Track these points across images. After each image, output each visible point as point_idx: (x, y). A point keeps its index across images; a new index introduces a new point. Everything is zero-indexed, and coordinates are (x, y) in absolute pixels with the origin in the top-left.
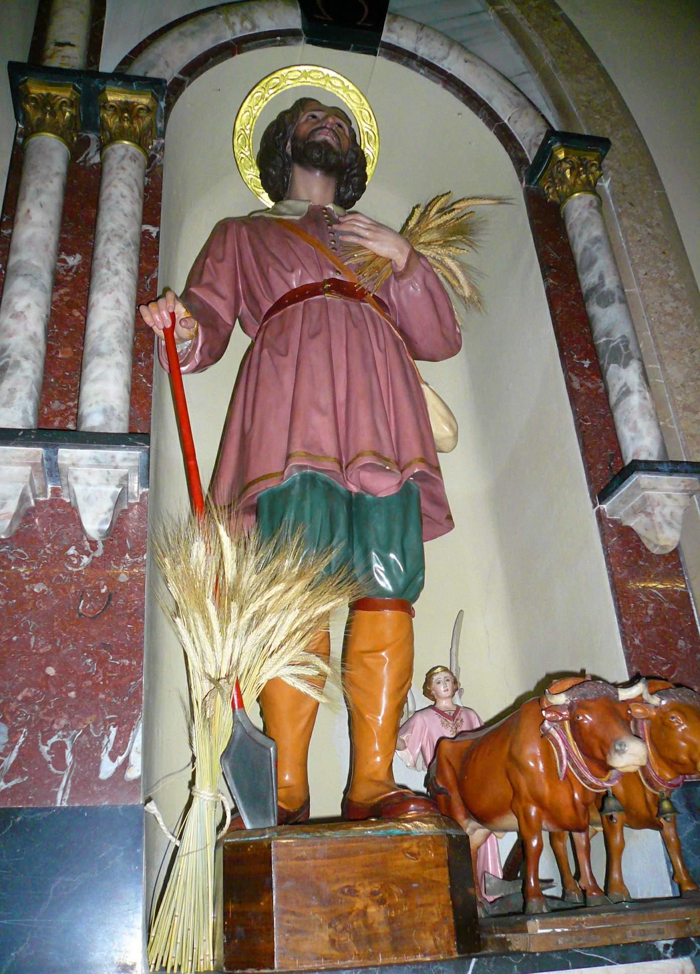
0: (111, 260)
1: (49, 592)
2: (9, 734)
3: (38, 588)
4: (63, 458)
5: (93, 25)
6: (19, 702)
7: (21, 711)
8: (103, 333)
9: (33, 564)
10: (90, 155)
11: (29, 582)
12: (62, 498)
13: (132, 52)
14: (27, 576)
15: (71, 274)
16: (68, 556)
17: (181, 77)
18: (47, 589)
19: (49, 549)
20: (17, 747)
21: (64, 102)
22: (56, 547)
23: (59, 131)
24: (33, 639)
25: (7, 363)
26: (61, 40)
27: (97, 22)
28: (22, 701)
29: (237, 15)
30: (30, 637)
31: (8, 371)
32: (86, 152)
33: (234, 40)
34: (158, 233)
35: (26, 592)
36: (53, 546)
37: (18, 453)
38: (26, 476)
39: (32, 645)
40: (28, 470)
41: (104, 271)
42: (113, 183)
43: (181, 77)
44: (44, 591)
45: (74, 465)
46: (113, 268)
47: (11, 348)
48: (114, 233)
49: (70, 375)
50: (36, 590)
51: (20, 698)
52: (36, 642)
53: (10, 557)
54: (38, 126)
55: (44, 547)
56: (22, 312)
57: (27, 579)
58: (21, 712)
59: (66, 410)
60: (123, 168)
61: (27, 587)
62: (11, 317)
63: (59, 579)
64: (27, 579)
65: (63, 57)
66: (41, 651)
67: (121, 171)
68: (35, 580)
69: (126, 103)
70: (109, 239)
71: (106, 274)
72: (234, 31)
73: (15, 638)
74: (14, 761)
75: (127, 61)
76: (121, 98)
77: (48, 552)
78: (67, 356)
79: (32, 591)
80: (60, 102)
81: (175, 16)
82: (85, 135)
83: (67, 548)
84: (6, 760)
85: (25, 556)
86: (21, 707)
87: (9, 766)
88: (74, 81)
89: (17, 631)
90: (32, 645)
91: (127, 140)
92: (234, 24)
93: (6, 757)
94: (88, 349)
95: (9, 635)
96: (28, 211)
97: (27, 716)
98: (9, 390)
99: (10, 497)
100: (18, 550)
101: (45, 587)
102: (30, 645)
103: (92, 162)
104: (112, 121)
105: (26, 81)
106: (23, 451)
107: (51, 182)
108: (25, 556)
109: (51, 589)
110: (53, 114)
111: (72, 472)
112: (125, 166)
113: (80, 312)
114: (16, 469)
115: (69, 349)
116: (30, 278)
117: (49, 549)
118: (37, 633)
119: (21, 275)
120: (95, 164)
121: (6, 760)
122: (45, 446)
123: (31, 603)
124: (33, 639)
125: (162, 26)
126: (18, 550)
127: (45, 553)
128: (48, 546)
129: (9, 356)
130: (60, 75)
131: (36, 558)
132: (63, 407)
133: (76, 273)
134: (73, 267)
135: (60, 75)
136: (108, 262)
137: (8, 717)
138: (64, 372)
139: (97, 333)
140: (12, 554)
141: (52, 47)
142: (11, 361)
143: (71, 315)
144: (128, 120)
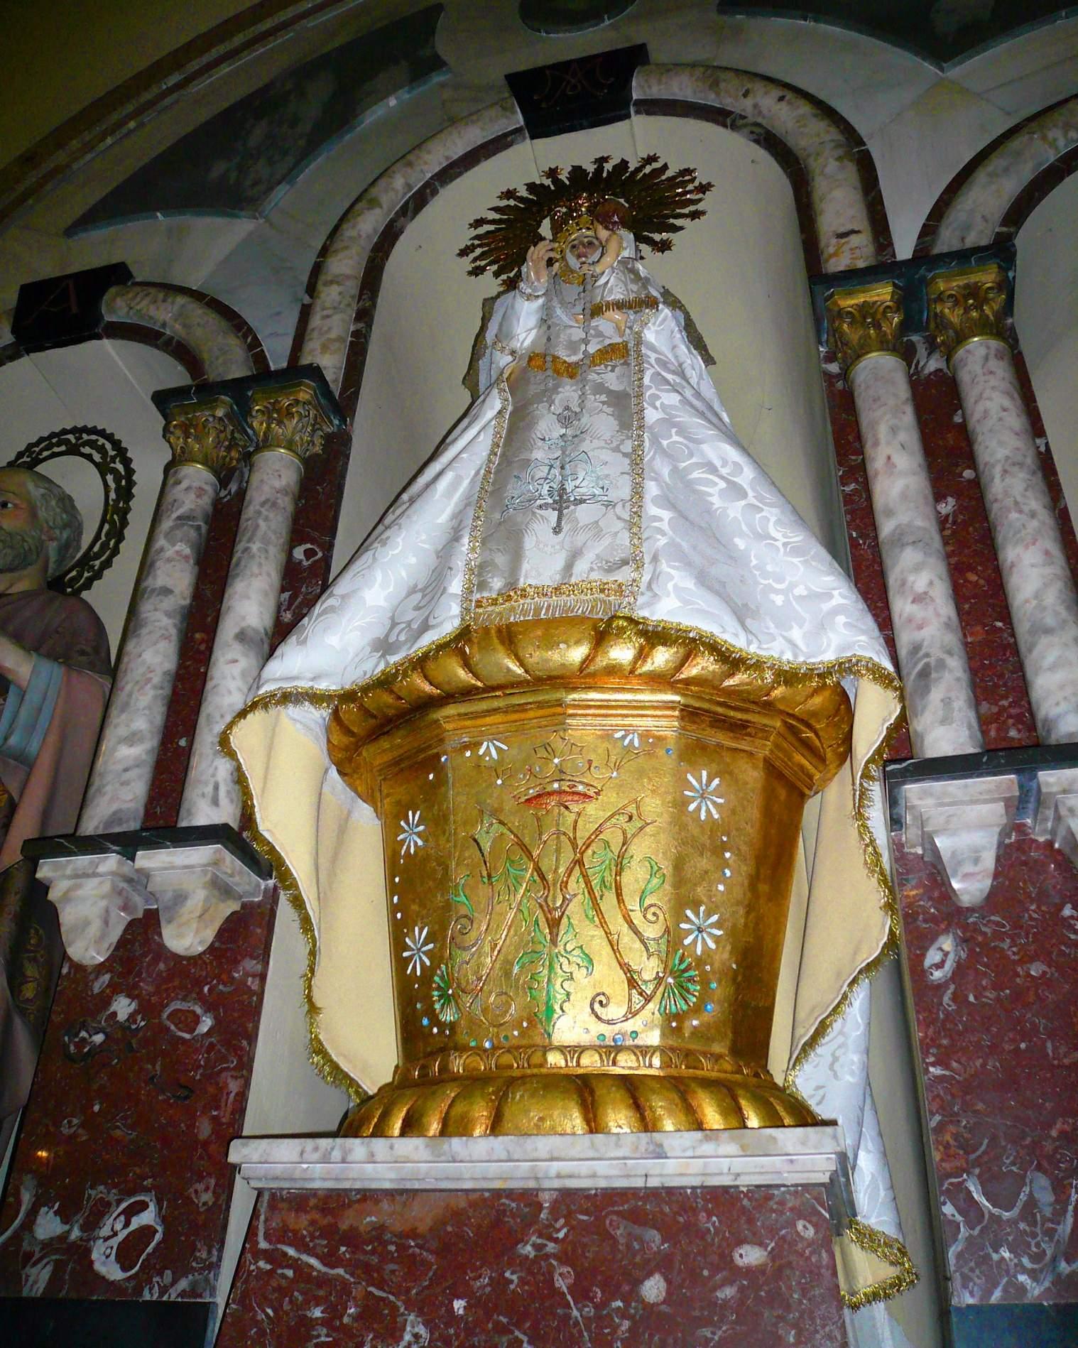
0: (1019, 499)
1: (1052, 974)
2: (1054, 1189)
3: (1036, 970)
4: (1048, 784)
5: (870, 198)
6: (1054, 1140)
7: (1060, 1154)
8: (1042, 601)
9: (1019, 936)
10: (922, 364)
11: (1021, 962)
12: (1032, 836)
13: (930, 217)
14: (1014, 953)
15: (948, 526)
16: (1065, 919)
17: (1004, 229)
18: (1048, 970)
19: (1034, 911)
20: (1071, 1208)
21: (888, 307)
22: (1044, 908)
23: (890, 345)
24: (1049, 1045)
25: (927, 665)
26: (842, 230)
27: (873, 194)
28: (1058, 1138)
29: (1055, 126)
30: (1044, 1042)
31: (934, 675)
32: (915, 362)
33: (1057, 160)
34: (1047, 444)
35: (1019, 976)
36: (1039, 907)
37: (984, 787)
38: (1002, 816)
39: (1051, 1054)
40: (1000, 807)
41: (1014, 515)
42: (985, 395)
43: (1004, 229)
44: (1044, 973)
45: (1065, 792)
46: (1026, 509)
47: (926, 643)
48: (1010, 461)
49: (990, 664)
50: (1033, 973)
51: (1054, 1133)
52: (1055, 1049)
53: (984, 929)
54: (862, 347)
55: (1027, 910)
56: (926, 593)
57: (1016, 957)
58: (1063, 1155)
59: (999, 714)
60: (991, 373)
61: (1019, 969)
62: (913, 602)
63: (1062, 953)
64: (1016, 957)
65: (851, 249)
66: (1066, 1061)
67: (991, 377)
68: (1028, 959)
69: (967, 286)
70: (1005, 471)
71: (1018, 519)
72: (1056, 148)
73: (1023, 1046)
74: (1073, 1230)
75: (929, 230)
76: (958, 283)
77: (1035, 916)
78: (980, 638)
79: (1030, 976)
80: (881, 309)
81: (968, 157)
82: (905, 339)
83: (1061, 909)
84: (1060, 1228)
85: (1004, 926)
86: (1060, 1147)
87: (1067, 1239)
88: (893, 278)
89: (1024, 1036)
90: (1051, 1054)
91: (975, 336)
92: (1055, 140)
93: (1059, 1224)
94: (1023, 628)
95: (1013, 1040)
96: (889, 458)
97: (1072, 1160)
98: (942, 701)
99: (984, 848)
100: (993, 918)
101: (1044, 968)
102: (1048, 1054)
103: (926, 372)
104: (954, 316)
105: (832, 295)
106: (990, 782)
107: (904, 413)
108: (1004, 926)
109: (1053, 969)
110: (877, 326)
111: (1064, 803)
112: (993, 369)
113: (976, 574)
114: (985, 809)
115: (979, 628)
116: (921, 544)
117: (1034, 911)
118: (1052, 1035)
119: (907, 544)
120: (931, 374)
121: (1060, 1228)
122: (1017, 772)
123: (1032, 993)
124: (1049, 1045)
125: (957, 171)
126: (993, 918)
127: (1031, 918)
128: (1033, 907)
129: (927, 655)
130: (855, 278)
131: (1021, 927)
132: (995, 709)
133: (954, 523)
134: (947, 516)
135: (855, 278)
136: (1016, 503)
137: (1045, 1164)
138: (981, 661)
139: (1034, 603)
140: (985, 925)
141: (834, 241)
142: (932, 660)
143: (966, 581)
144: (975, 308)
